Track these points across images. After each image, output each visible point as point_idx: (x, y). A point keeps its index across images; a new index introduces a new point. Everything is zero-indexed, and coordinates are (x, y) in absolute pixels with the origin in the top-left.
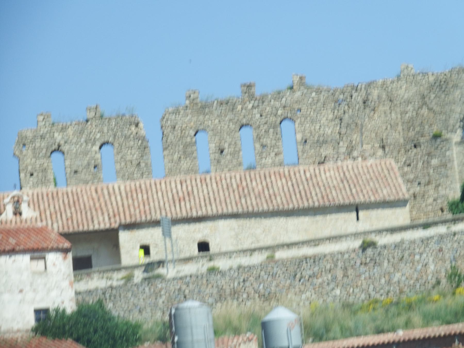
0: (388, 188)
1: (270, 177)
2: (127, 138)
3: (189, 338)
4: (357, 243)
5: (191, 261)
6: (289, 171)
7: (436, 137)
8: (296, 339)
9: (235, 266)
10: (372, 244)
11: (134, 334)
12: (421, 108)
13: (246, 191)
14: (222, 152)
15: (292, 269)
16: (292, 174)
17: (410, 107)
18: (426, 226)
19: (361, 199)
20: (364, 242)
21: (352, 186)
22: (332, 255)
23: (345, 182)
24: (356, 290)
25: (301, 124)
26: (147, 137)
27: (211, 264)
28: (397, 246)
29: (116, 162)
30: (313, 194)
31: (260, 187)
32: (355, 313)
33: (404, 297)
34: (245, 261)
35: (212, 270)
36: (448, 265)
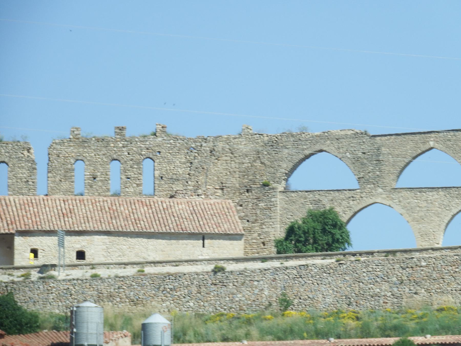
0: (228, 224)
1: (135, 204)
2: (19, 159)
3: (85, 331)
4: (210, 267)
5: (77, 268)
6: (150, 202)
7: (265, 185)
8: (167, 339)
9: (113, 275)
10: (222, 269)
11: (36, 322)
12: (254, 161)
13: (116, 214)
14: (95, 178)
15: (157, 282)
16: (152, 203)
17: (247, 160)
18: (264, 260)
19: (207, 230)
20: (215, 268)
21: (200, 219)
22: (190, 274)
23: (194, 215)
24: (206, 304)
25: (160, 163)
26: (36, 161)
27: (94, 271)
28: (241, 273)
29: (9, 178)
30: (170, 222)
31: (127, 212)
32: (205, 322)
33: (242, 313)
34: (121, 272)
35: (95, 276)
36: (279, 292)
